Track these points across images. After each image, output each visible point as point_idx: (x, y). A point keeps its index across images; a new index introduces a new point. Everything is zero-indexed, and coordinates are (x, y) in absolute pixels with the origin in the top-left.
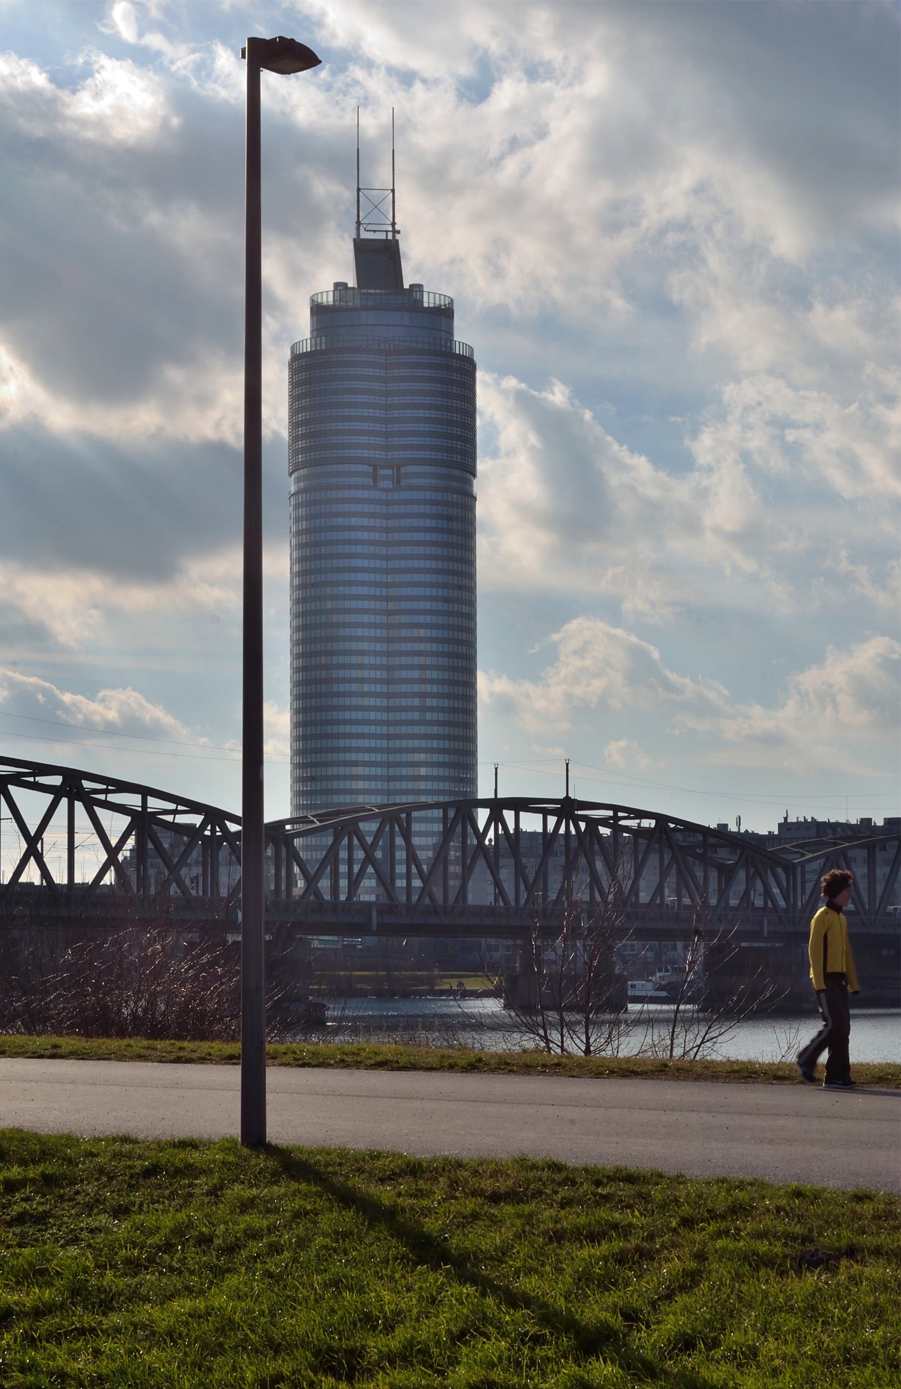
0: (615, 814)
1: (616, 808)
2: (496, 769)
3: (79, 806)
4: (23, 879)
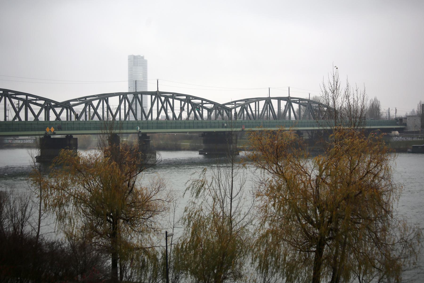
0: (202, 102)
1: (202, 100)
2: (158, 81)
3: (7, 98)
4: (16, 120)
